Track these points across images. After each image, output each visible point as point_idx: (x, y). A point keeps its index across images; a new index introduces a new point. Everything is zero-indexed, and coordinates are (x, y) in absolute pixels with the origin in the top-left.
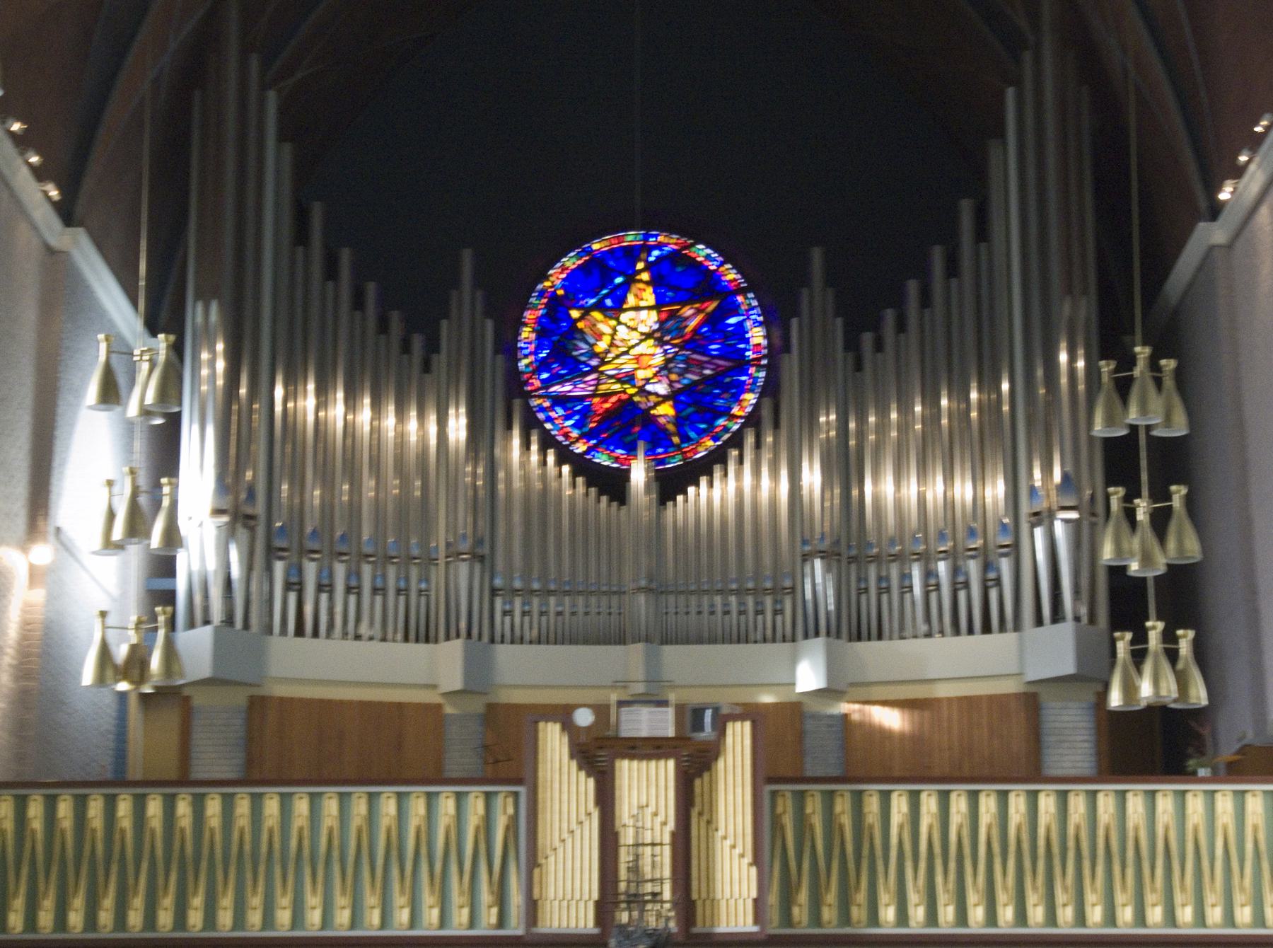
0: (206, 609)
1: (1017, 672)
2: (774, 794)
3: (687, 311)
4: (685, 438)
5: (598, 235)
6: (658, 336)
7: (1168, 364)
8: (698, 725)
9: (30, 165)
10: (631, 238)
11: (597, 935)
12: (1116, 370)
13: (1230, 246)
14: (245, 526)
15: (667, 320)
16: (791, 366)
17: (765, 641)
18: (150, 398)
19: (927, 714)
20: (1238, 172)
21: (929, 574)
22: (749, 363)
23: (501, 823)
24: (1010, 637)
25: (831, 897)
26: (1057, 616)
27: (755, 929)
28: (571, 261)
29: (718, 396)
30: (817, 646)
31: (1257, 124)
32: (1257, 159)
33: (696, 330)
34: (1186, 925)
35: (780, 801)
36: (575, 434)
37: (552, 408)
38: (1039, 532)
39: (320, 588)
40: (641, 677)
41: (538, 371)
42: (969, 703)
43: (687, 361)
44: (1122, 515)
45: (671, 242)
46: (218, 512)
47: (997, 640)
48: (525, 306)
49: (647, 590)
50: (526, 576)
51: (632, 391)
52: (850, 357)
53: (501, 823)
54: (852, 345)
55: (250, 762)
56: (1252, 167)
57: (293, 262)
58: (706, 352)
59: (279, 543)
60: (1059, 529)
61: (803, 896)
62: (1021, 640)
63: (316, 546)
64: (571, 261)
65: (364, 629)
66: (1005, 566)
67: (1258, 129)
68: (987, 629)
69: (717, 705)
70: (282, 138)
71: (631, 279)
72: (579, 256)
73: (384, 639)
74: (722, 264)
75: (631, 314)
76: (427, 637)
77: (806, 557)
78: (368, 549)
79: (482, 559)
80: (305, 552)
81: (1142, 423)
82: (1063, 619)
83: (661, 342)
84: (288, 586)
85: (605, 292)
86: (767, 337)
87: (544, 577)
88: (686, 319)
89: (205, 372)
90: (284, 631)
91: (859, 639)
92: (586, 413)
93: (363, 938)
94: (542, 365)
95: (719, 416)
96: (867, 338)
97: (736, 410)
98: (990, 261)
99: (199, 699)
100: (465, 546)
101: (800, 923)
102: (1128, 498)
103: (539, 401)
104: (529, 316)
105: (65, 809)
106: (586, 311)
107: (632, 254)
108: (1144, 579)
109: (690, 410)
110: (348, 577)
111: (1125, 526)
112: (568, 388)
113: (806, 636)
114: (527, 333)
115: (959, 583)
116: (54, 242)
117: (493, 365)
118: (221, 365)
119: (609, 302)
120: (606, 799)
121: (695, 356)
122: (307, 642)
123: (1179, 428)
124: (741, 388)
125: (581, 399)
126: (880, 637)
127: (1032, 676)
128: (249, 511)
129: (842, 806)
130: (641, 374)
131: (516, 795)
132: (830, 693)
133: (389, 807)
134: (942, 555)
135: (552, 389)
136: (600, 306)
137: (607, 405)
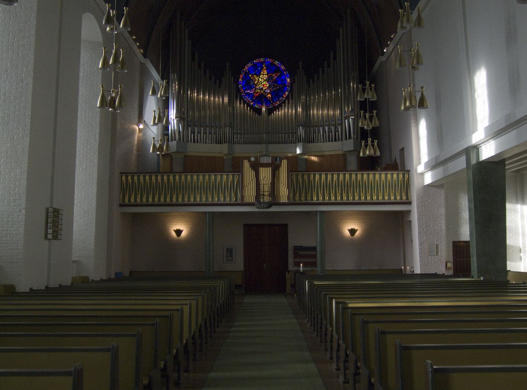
0: (175, 137)
2: (292, 174)
3: (274, 75)
5: (255, 59)
6: (268, 80)
7: (373, 85)
8: (276, 160)
10: (262, 60)
12: (362, 87)
14: (183, 120)
15: (269, 77)
20: (388, 46)
22: (287, 86)
23: (236, 180)
24: (340, 142)
26: (350, 138)
27: (288, 201)
28: (249, 65)
29: (280, 93)
31: (392, 35)
32: (392, 43)
38: (346, 121)
39: (198, 133)
42: (331, 156)
43: (274, 85)
45: (270, 60)
48: (240, 74)
49: (266, 133)
53: (236, 180)
54: (308, 82)
64: (249, 65)
65: (207, 141)
66: (339, 128)
68: (335, 140)
71: (262, 68)
73: (212, 143)
76: (220, 143)
79: (231, 127)
80: (195, 125)
83: (268, 82)
84: (191, 132)
88: (273, 77)
91: (309, 143)
96: (311, 80)
100: (228, 124)
102: (364, 113)
106: (252, 76)
107: (262, 63)
108: (368, 130)
111: (364, 119)
113: (298, 142)
115: (330, 131)
116: (142, 61)
123: (375, 99)
126: (314, 142)
128: (183, 117)
129: (306, 177)
131: (239, 175)
136: (255, 74)
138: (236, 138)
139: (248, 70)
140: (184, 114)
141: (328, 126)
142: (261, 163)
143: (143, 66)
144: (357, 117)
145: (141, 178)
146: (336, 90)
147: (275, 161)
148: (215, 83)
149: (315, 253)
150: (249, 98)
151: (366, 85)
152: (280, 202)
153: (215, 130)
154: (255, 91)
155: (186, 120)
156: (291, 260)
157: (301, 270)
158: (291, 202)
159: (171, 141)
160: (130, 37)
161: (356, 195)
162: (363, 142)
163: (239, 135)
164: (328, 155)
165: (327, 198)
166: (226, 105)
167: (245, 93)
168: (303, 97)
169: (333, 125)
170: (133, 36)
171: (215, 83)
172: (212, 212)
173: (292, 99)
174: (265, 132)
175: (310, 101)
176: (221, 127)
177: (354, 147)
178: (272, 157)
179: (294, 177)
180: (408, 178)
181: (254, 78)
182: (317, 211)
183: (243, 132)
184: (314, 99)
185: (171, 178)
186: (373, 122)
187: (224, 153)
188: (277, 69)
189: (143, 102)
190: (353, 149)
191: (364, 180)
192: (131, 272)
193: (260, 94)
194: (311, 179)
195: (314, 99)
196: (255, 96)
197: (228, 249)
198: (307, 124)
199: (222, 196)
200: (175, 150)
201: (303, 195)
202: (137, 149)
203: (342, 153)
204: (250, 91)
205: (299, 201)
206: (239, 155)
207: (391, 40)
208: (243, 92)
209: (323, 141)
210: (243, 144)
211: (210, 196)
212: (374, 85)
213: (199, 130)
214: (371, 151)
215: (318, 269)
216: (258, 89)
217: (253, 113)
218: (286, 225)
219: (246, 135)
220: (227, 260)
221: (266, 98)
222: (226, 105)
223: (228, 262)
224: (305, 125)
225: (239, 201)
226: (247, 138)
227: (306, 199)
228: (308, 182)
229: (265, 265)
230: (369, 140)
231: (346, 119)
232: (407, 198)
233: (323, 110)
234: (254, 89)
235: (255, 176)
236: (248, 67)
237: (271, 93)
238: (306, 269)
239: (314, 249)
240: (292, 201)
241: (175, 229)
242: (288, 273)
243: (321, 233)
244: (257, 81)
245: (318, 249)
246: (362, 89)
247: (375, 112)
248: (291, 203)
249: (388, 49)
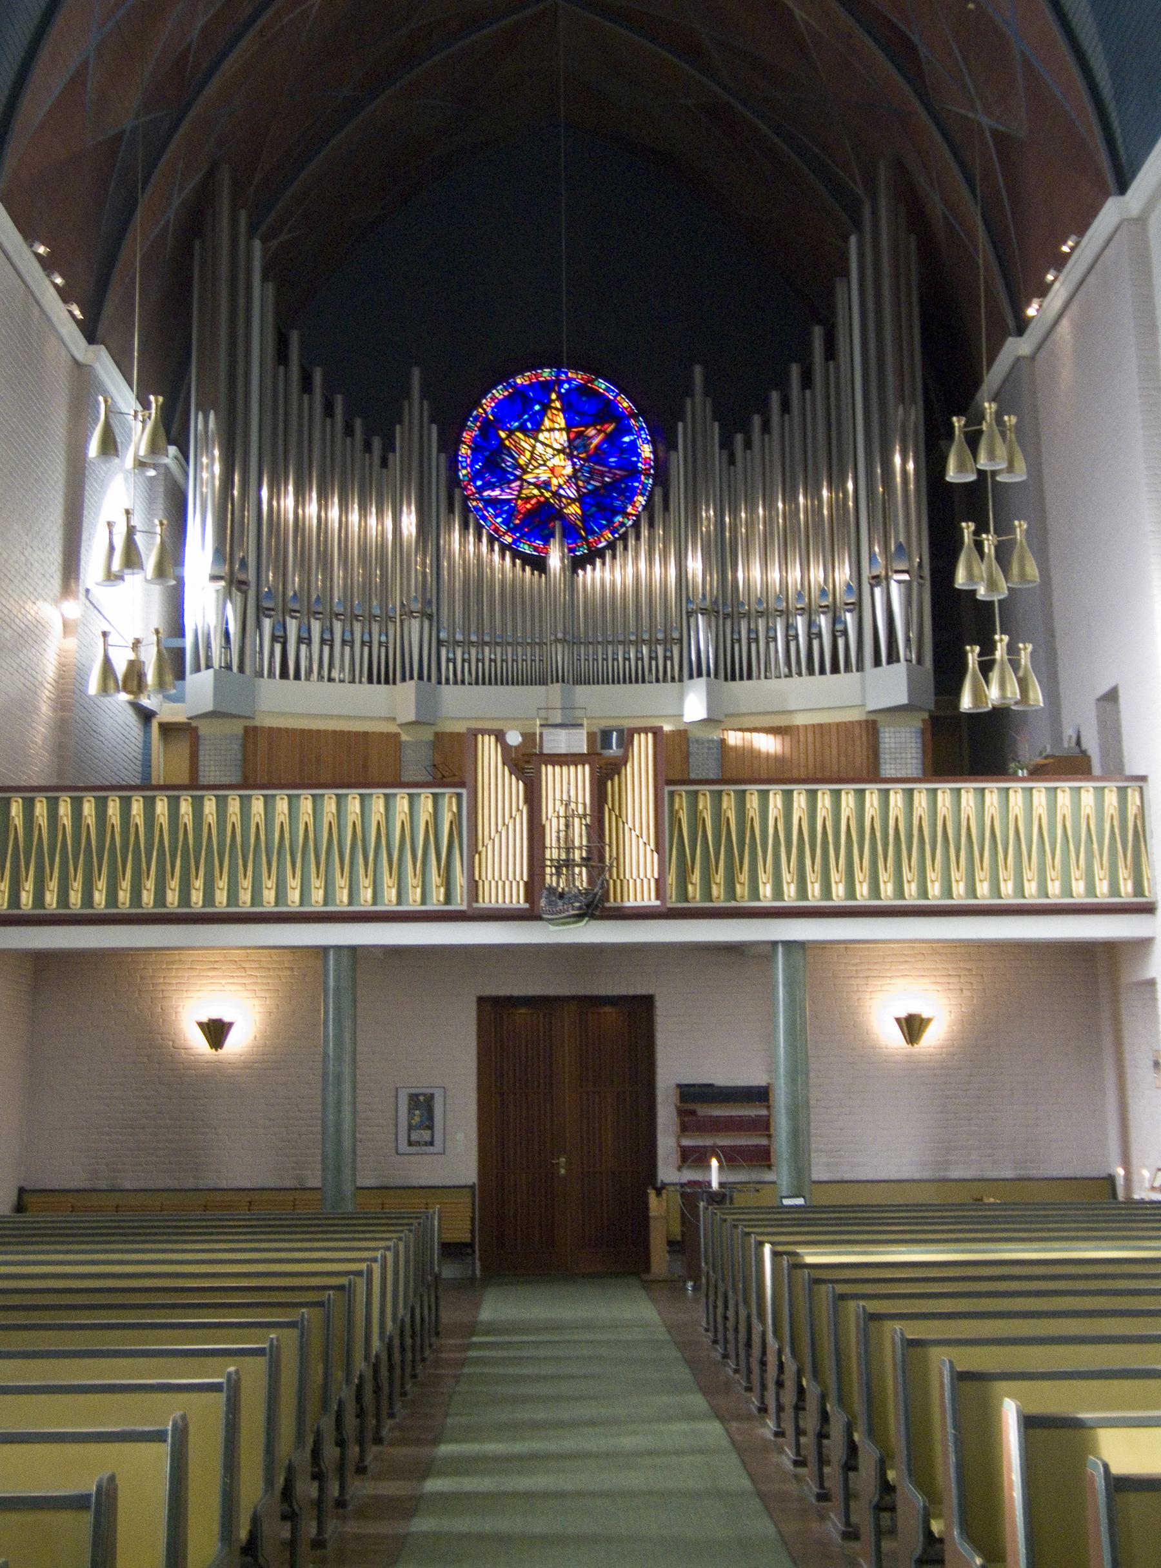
0: (208, 658)
1: (860, 703)
2: (672, 794)
3: (591, 432)
4: (590, 532)
5: (521, 372)
6: (569, 452)
7: (1010, 420)
8: (607, 744)
9: (38, 256)
10: (546, 374)
11: (526, 909)
12: (966, 426)
13: (1032, 358)
14: (239, 590)
15: (575, 439)
16: (678, 462)
17: (658, 681)
18: (142, 452)
19: (788, 738)
20: (1043, 290)
21: (788, 627)
22: (640, 473)
23: (447, 818)
24: (855, 675)
25: (719, 877)
26: (893, 658)
27: (658, 903)
28: (499, 393)
29: (616, 499)
30: (700, 685)
31: (1065, 243)
32: (1061, 278)
33: (598, 447)
34: (1008, 896)
35: (677, 799)
36: (503, 528)
37: (485, 508)
38: (878, 591)
39: (300, 641)
40: (559, 705)
41: (473, 480)
42: (821, 729)
43: (591, 471)
44: (972, 545)
45: (578, 377)
46: (215, 578)
47: (844, 679)
48: (463, 428)
49: (564, 641)
50: (466, 630)
51: (548, 495)
52: (725, 452)
53: (447, 818)
54: (726, 443)
55: (245, 778)
56: (1057, 285)
57: (275, 377)
58: (605, 463)
59: (267, 604)
60: (895, 589)
61: (696, 877)
62: (863, 680)
63: (297, 607)
64: (499, 393)
65: (335, 674)
66: (849, 618)
67: (1065, 249)
68: (835, 669)
69: (621, 728)
70: (265, 278)
71: (546, 407)
72: (505, 389)
73: (353, 681)
74: (618, 395)
75: (546, 434)
76: (388, 680)
77: (689, 614)
78: (338, 609)
79: (430, 617)
80: (287, 611)
81: (988, 467)
82: (898, 660)
83: (570, 457)
84: (274, 639)
85: (526, 417)
86: (654, 452)
87: (480, 631)
88: (589, 438)
89: (205, 475)
90: (271, 674)
91: (733, 679)
92: (512, 512)
93: (335, 912)
94: (476, 475)
95: (616, 515)
96: (739, 438)
97: (630, 510)
98: (838, 378)
99: (204, 729)
100: (416, 606)
101: (694, 898)
102: (977, 533)
103: (475, 503)
104: (466, 436)
105: (89, 808)
106: (511, 433)
107: (546, 388)
108: (992, 602)
109: (594, 509)
110: (322, 632)
111: (976, 554)
112: (497, 492)
113: (691, 677)
114: (464, 450)
115: (813, 634)
116: (80, 357)
117: (437, 461)
118: (217, 469)
119: (529, 425)
120: (533, 798)
121: (597, 467)
122: (291, 683)
123: (1019, 475)
124: (633, 492)
125: (508, 501)
126: (750, 677)
127: (871, 707)
128: (242, 577)
129: (729, 804)
130: (554, 482)
131: (459, 796)
132: (709, 721)
133: (354, 806)
134: (799, 612)
135: (485, 494)
136: (523, 429)
137: (528, 506)
138: (448, 660)
139: (493, 413)
140: (244, 564)
141: (808, 612)
142: (545, 751)
143: (82, 373)
144: (921, 577)
145: (65, 809)
146: (838, 484)
147: (603, 748)
148: (368, 447)
149: (764, 1112)
150: (499, 520)
151: (983, 418)
152: (627, 904)
153: (367, 630)
154: (520, 492)
155: (252, 594)
156: (667, 1143)
157: (715, 1185)
158: (669, 905)
159: (191, 673)
160: (25, 247)
161: (931, 875)
162: (972, 651)
163: (459, 651)
164: (806, 726)
165: (814, 888)
166: (409, 546)
167: (482, 499)
168: (708, 514)
169: (825, 609)
170: (36, 245)
171: (368, 447)
172: (353, 949)
173: (666, 508)
174: (560, 635)
175: (736, 531)
176: (391, 619)
177: (911, 693)
178: (591, 736)
179: (682, 805)
180: (1142, 808)
181: (517, 445)
182: (774, 944)
183: (474, 638)
184: (752, 521)
185: (185, 808)
186: (1015, 569)
187: (399, 721)
188: (604, 411)
189: (81, 515)
190: (903, 699)
191: (963, 816)
192: (22, 1191)
193: (538, 500)
194: (751, 813)
195: (751, 523)
196: (519, 512)
197: (414, 1098)
198: (724, 604)
199: (391, 884)
200: (209, 707)
201: (719, 877)
202: (58, 697)
203: (863, 717)
204: (502, 491)
205: (701, 901)
206: (460, 727)
207: (1060, 262)
208: (473, 494)
209: (786, 670)
210: (477, 683)
211: (341, 882)
212: (1014, 420)
213: (305, 628)
214: (1008, 688)
215: (781, 1175)
216: (529, 483)
217: (514, 564)
218: (647, 1002)
219: (487, 649)
220: (410, 1144)
221: (562, 517)
222: (409, 546)
223: (413, 1149)
224: (717, 612)
225: (460, 903)
226: (491, 660)
227: (731, 893)
228: (737, 824)
229: (563, 1160)
230: (1001, 640)
231: (878, 584)
232: (1139, 890)
233: (785, 564)
234: (518, 483)
235: (526, 801)
236: (492, 399)
237: (581, 499)
238: (732, 1178)
239: (761, 1095)
240: (673, 903)
241: (205, 1019)
242: (659, 1191)
243: (791, 1032)
244: (528, 454)
245: (781, 1099)
246: (966, 434)
247: (1020, 527)
248: (670, 909)
249: (1045, 304)
